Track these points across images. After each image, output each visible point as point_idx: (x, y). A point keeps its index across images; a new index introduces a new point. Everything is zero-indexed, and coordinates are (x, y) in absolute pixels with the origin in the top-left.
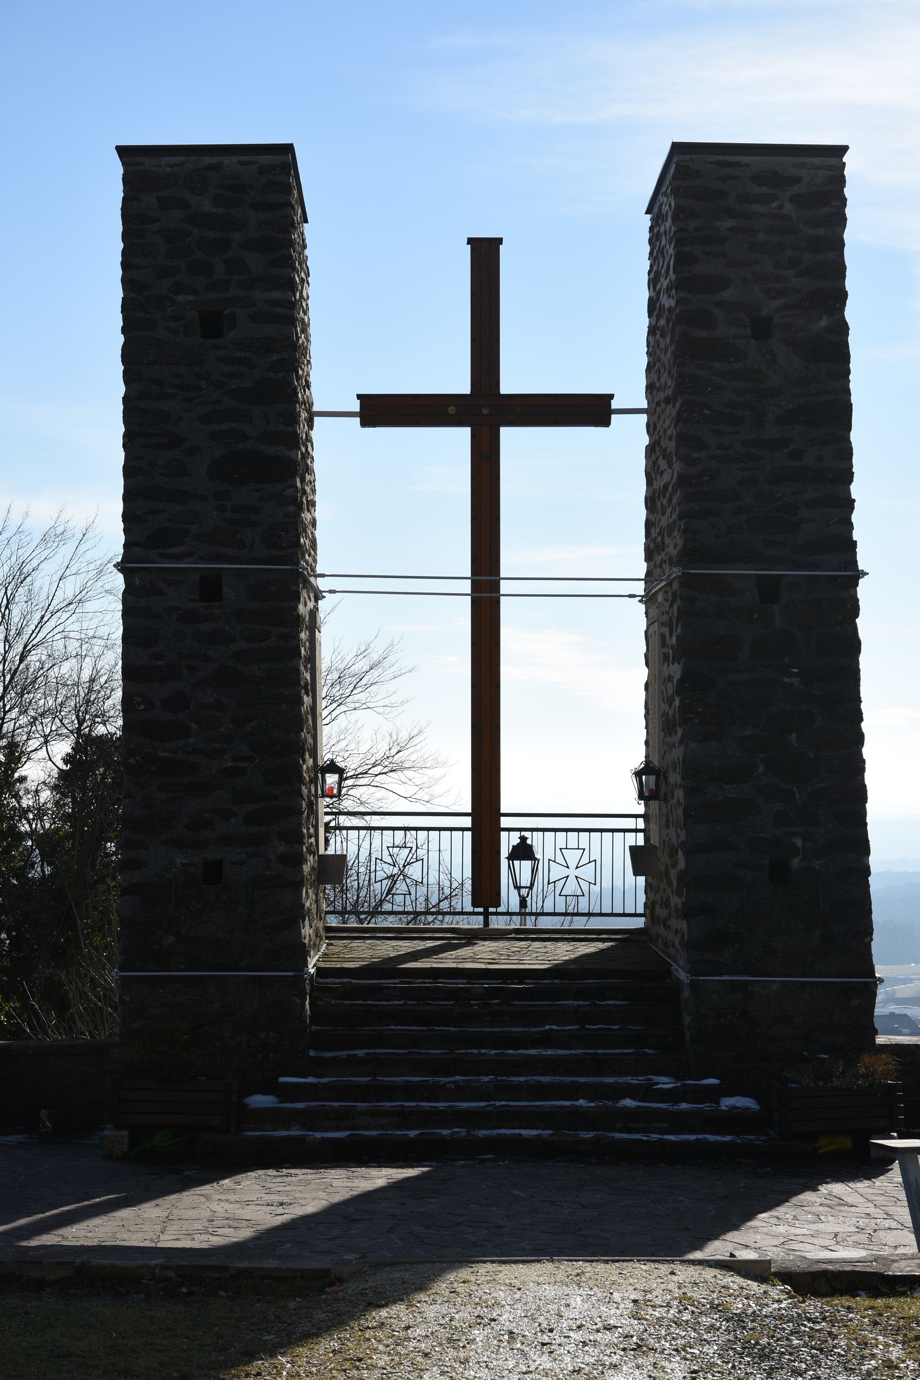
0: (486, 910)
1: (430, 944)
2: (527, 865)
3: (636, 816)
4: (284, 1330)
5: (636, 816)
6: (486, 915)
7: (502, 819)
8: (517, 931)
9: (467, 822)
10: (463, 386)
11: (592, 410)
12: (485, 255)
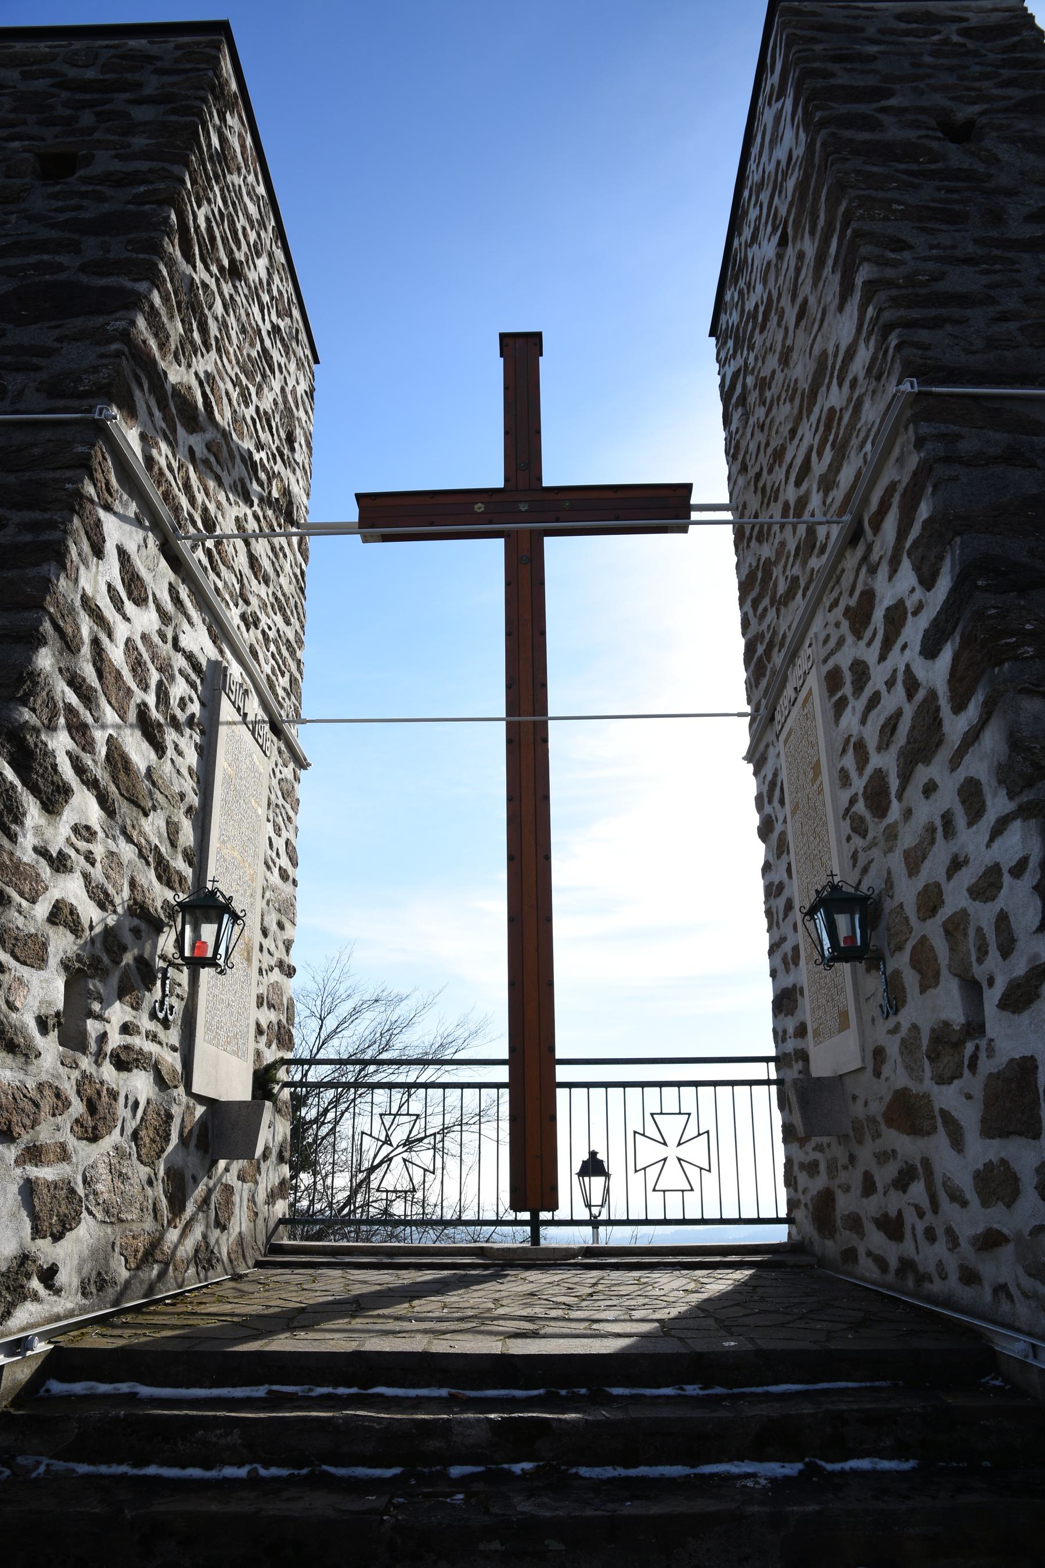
0: (535, 1216)
1: (429, 1275)
2: (598, 1182)
3: (766, 1060)
5: (766, 1060)
6: (535, 1224)
7: (559, 1068)
8: (588, 1252)
9: (502, 1074)
10: (494, 478)
11: (661, 508)
12: (521, 353)
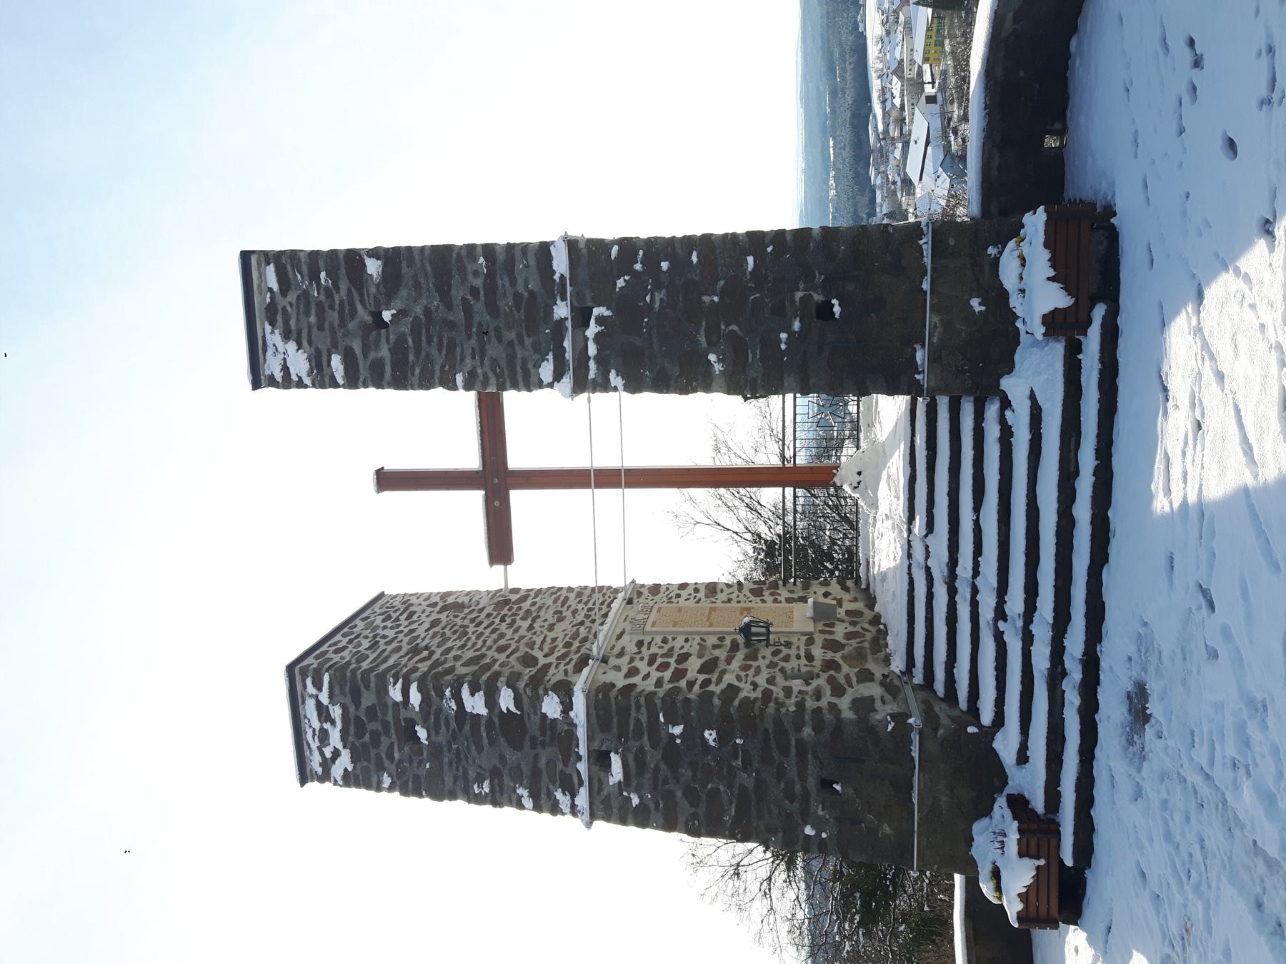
4: (468, 309)
12: (387, 480)
